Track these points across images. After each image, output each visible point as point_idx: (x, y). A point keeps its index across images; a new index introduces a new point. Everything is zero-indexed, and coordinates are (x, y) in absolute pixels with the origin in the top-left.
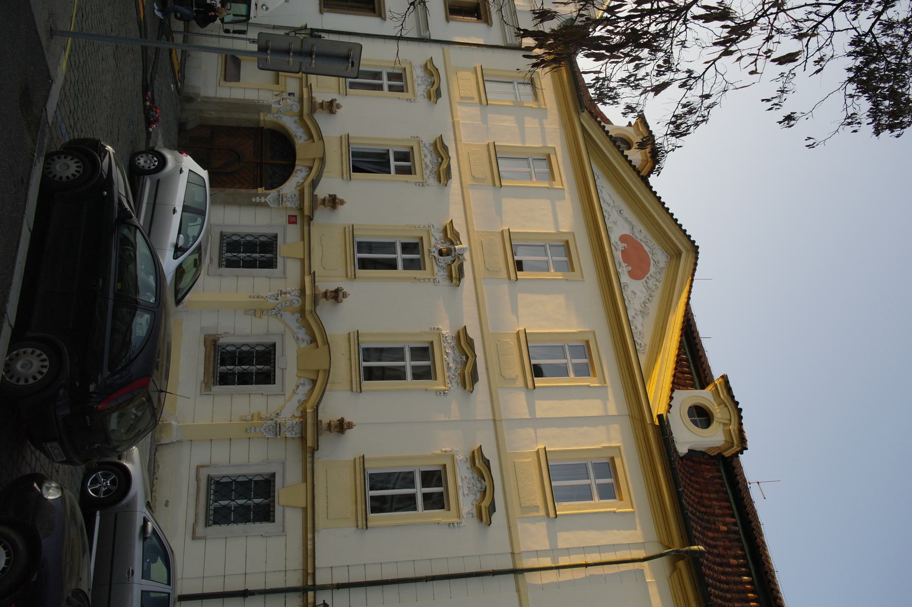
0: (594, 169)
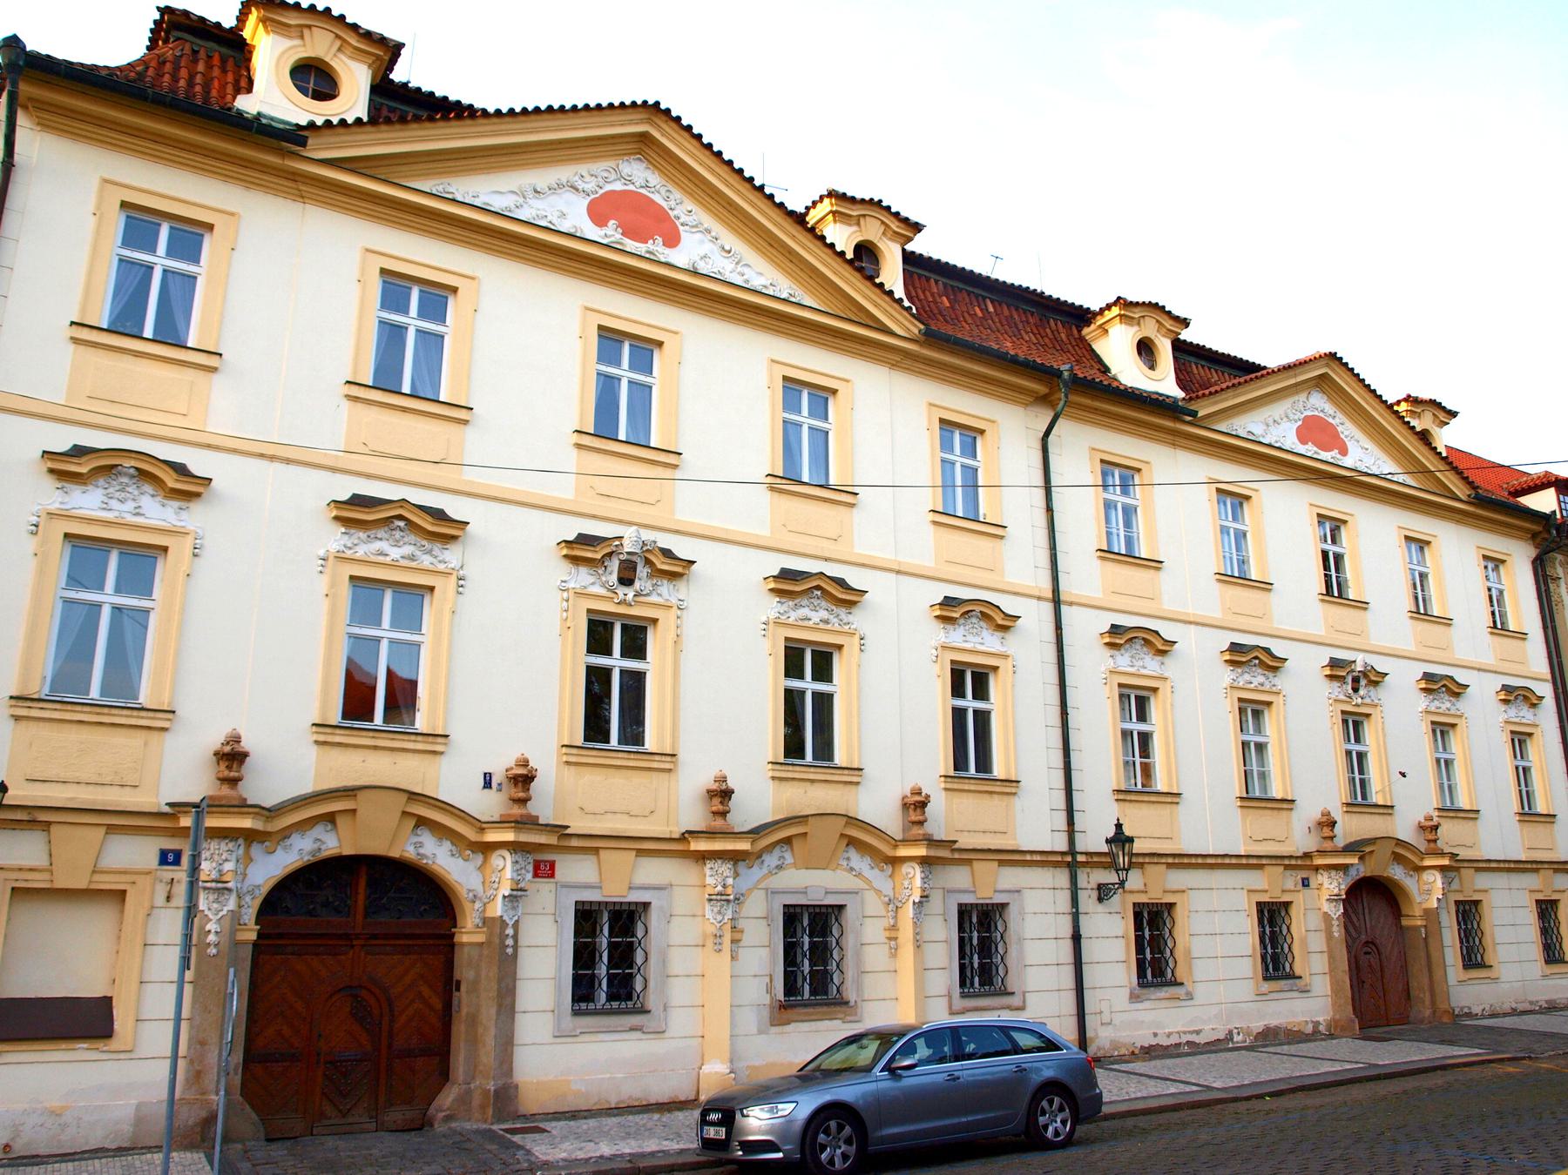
0: (428, 188)
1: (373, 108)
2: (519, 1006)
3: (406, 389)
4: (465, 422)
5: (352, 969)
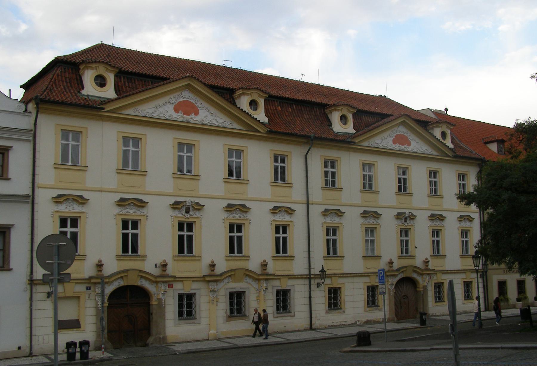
2: (166, 318)
5: (129, 310)
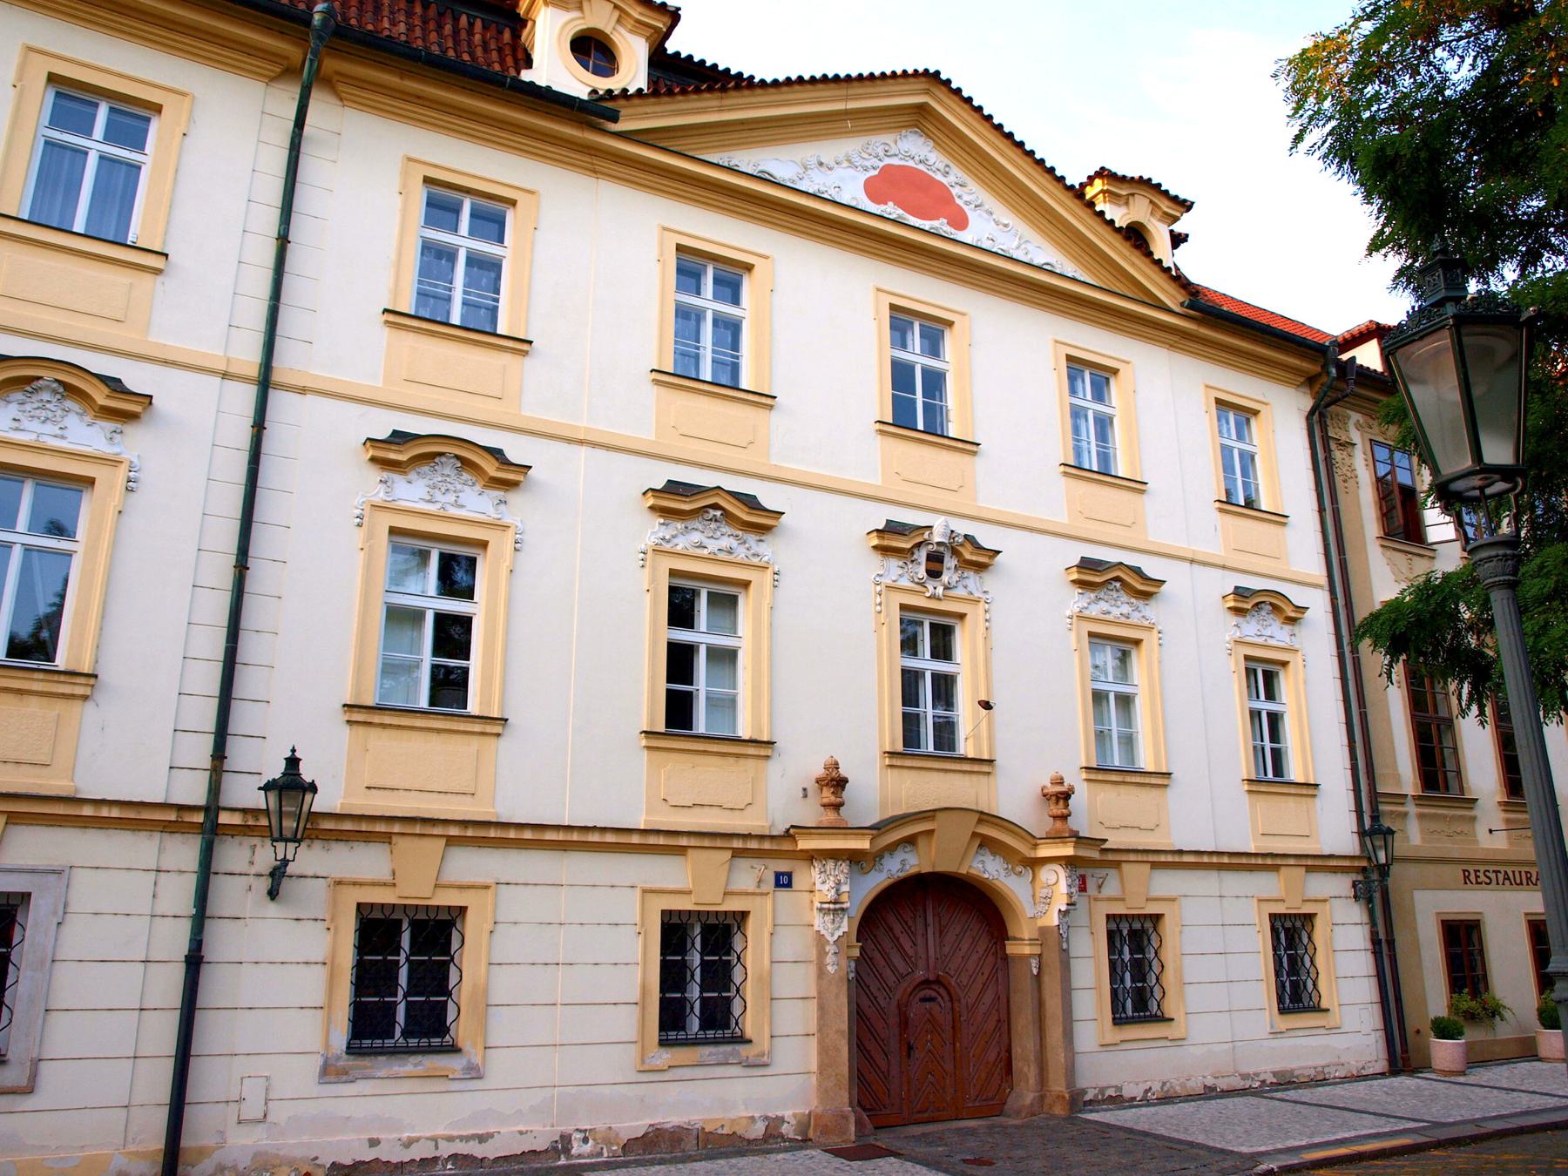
1: (652, 81)
3: (79, 226)
4: (157, 272)
